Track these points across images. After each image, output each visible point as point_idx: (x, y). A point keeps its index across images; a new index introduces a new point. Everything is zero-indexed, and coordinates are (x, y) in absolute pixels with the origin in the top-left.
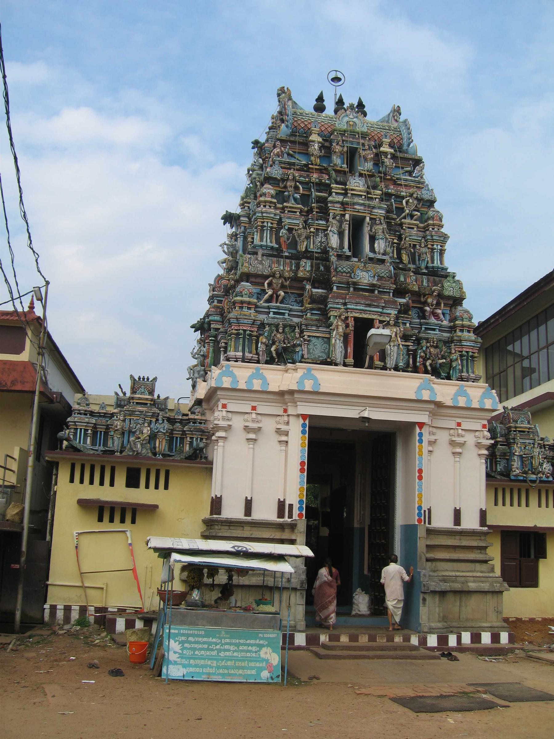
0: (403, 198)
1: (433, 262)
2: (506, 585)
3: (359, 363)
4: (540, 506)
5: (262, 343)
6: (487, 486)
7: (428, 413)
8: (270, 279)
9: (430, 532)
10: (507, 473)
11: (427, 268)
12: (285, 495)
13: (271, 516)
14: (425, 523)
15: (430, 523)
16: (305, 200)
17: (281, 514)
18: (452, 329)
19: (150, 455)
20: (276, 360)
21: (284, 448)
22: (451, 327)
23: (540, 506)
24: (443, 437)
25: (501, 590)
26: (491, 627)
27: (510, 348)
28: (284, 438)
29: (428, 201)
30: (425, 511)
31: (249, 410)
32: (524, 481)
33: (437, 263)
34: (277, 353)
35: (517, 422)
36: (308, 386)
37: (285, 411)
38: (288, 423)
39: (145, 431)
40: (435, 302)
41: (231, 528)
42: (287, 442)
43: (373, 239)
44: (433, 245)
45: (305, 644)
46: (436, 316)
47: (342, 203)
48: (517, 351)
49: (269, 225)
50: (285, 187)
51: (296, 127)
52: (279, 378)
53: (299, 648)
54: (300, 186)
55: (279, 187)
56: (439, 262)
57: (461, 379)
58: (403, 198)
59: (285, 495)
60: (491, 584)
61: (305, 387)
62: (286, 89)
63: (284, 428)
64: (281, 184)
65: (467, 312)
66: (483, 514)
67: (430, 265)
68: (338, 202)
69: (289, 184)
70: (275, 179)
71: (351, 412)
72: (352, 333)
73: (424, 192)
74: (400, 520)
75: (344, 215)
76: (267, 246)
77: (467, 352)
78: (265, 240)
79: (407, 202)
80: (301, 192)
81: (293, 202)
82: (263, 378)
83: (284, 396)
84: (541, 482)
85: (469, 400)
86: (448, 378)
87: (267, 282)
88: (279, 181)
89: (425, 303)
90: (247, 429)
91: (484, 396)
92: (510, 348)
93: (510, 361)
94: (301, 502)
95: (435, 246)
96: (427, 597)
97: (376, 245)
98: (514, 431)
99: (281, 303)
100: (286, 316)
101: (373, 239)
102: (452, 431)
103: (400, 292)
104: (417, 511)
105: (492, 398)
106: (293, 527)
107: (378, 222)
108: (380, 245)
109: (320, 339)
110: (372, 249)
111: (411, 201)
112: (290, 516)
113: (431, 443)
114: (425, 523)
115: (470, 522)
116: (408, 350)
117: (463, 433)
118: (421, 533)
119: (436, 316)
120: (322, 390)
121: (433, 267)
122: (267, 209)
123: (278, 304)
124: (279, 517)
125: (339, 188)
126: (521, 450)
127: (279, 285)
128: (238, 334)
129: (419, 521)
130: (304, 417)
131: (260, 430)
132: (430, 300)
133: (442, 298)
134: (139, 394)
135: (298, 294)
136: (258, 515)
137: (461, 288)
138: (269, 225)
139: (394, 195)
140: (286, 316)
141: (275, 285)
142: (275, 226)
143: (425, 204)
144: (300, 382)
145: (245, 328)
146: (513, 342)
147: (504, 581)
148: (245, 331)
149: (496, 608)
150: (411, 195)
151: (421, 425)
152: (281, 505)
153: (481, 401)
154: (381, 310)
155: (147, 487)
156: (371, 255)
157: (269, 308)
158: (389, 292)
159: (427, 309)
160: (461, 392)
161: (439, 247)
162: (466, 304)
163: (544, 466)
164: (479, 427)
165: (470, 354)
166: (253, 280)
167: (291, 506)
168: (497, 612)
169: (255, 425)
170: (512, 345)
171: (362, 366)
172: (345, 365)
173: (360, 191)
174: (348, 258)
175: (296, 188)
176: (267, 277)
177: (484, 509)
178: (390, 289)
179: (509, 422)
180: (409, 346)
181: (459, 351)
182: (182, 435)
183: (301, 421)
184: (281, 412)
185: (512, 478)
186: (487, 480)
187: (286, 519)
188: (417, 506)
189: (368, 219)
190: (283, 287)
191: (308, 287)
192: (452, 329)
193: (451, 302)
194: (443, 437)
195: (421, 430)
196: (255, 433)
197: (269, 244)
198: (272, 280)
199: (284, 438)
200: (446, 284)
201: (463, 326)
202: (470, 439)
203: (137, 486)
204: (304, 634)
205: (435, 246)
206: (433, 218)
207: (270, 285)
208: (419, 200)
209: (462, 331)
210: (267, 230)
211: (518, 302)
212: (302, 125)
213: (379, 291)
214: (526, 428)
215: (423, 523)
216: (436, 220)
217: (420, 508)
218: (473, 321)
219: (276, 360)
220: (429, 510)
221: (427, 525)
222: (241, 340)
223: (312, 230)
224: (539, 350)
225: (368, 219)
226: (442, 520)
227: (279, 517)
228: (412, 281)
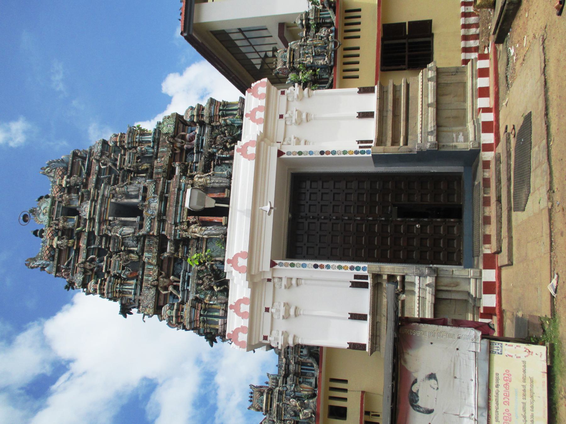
0: (100, 167)
1: (149, 142)
2: (430, 65)
3: (225, 212)
4: (359, 37)
5: (210, 301)
6: (341, 87)
7: (269, 147)
8: (159, 289)
9: (380, 141)
10: (329, 68)
11: (153, 148)
12: (347, 282)
13: (366, 295)
14: (370, 147)
15: (371, 142)
16: (101, 253)
17: (365, 286)
18: (202, 124)
19: (315, 399)
20: (226, 286)
21: (303, 281)
22: (201, 126)
23: (359, 37)
24: (294, 131)
25: (435, 69)
26: (472, 78)
27: (258, 67)
28: (294, 282)
29: (103, 146)
30: (360, 147)
31: (268, 315)
32: (335, 52)
33: (150, 138)
34: (220, 286)
35: (285, 62)
36: (243, 262)
37: (269, 280)
38: (281, 278)
39: (294, 403)
40: (180, 140)
41: (378, 334)
42: (298, 279)
43: (128, 196)
44: (136, 142)
45: (494, 270)
46: (192, 138)
47: (100, 223)
48: (259, 61)
49: (118, 286)
50: (92, 270)
51: (49, 258)
52: (239, 288)
53: (499, 276)
54: (91, 256)
55: (91, 275)
56: (150, 136)
57: (242, 116)
58: (100, 167)
59: (347, 282)
60: (429, 80)
61: (243, 266)
62: (27, 263)
63: (284, 282)
64: (88, 274)
65: (187, 111)
66: (364, 90)
67: (151, 145)
68: (99, 226)
69: (88, 267)
70: (83, 279)
71: (269, 222)
72: (200, 217)
73: (95, 150)
74: (371, 168)
75: (110, 221)
76: (135, 289)
77: (220, 110)
78: (130, 291)
79: (104, 164)
80: (94, 256)
81: (102, 264)
82: (240, 302)
83: (255, 282)
84: (336, 37)
85: (259, 108)
86: (240, 127)
87: (162, 291)
88: (86, 276)
89: (181, 148)
90: (287, 317)
91: (255, 95)
92: (258, 67)
93: (266, 67)
94: (352, 268)
95: (137, 140)
96: (441, 144)
97: (133, 193)
98: (293, 64)
99: (180, 278)
100: (190, 274)
101: (128, 196)
102: (288, 123)
103: (170, 173)
104: (360, 155)
105: (256, 87)
106: (377, 277)
107: (113, 192)
108: (132, 189)
109: (208, 245)
110: (136, 197)
111: (102, 161)
112: (366, 277)
113: (298, 142)
114: (370, 147)
115: (371, 102)
116: (218, 165)
117: (289, 112)
118: (380, 150)
119: (192, 138)
120: (247, 250)
121: (154, 142)
122: (106, 287)
123: (181, 280)
124: (367, 287)
125: (89, 225)
126: (309, 57)
127: (165, 280)
128: (204, 322)
129: (368, 152)
130: (273, 264)
131: (287, 304)
132: (178, 145)
133: (177, 134)
134: (262, 405)
135: (174, 262)
136: (366, 309)
137: (169, 117)
138: (118, 286)
139: (97, 176)
140: (190, 274)
141: (165, 284)
142: (119, 281)
143: (106, 148)
144: (240, 270)
145: (199, 315)
146: (253, 65)
147: (426, 67)
148: (201, 315)
149: (454, 73)
150: (98, 161)
151: (280, 153)
152: (355, 285)
153: (260, 97)
154: (181, 192)
155: (345, 399)
156: (140, 198)
157: (183, 291)
158: (168, 183)
159: (185, 146)
160: (252, 116)
161: (138, 137)
162: (182, 113)
163: (322, 35)
164: (284, 98)
165: (221, 108)
166: (161, 303)
167: (356, 277)
168: (457, 72)
169: (282, 309)
170: (256, 66)
171: (228, 209)
172: (226, 225)
173: (91, 206)
174: (142, 219)
175: (93, 260)
176: (158, 293)
177: (358, 90)
178: (165, 183)
179: (286, 68)
180: (214, 164)
181: (219, 118)
182: (299, 364)
183: (277, 267)
184: (271, 284)
185: (332, 63)
186: (335, 88)
187: (369, 281)
188: (354, 155)
189: (113, 200)
190: (167, 277)
191: (166, 255)
192: (202, 124)
193: (181, 126)
194: (294, 131)
195: (285, 153)
196: (290, 308)
197: (133, 287)
198: (161, 287)
199: (294, 282)
200: (165, 130)
201: (198, 115)
202: (295, 106)
203: (345, 409)
204: (483, 271)
205: (137, 140)
206: (115, 143)
207: (166, 288)
208: (102, 153)
209: (202, 116)
210: (122, 288)
211: (217, 64)
212: (48, 252)
213: (167, 193)
214: (290, 54)
215: (370, 149)
216: (116, 139)
217: (356, 152)
218: (194, 107)
219: (226, 286)
220: (359, 142)
221: (373, 145)
222: (209, 318)
223: (123, 248)
224: (251, 45)
225: (113, 200)
226: (369, 130)
227: (367, 287)
228: (161, 162)
